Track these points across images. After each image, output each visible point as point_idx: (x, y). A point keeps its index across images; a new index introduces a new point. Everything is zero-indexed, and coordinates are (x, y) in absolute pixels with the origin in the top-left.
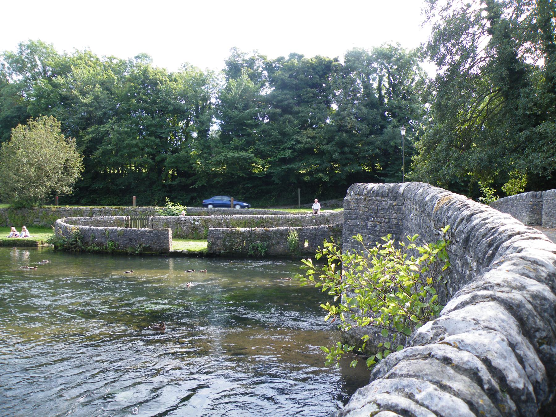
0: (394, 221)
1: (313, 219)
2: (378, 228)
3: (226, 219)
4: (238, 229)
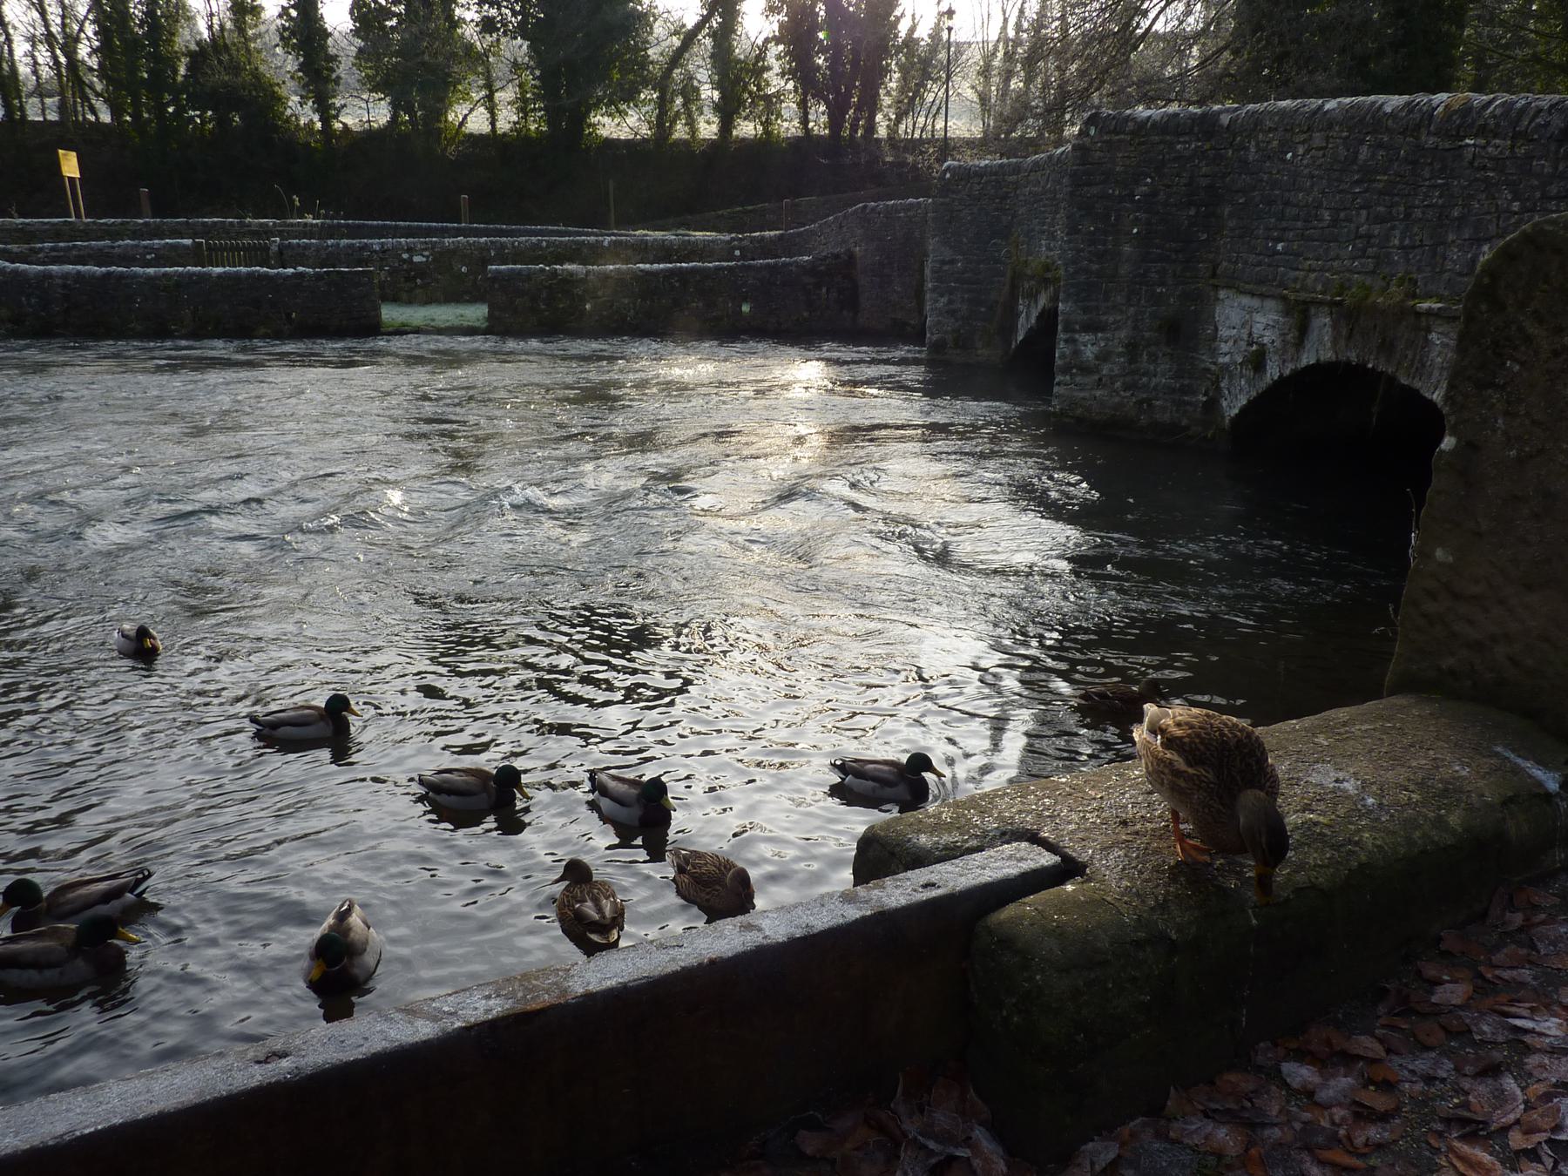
0: (1204, 182)
1: (734, 248)
2: (1162, 197)
3: (503, 246)
4: (568, 267)
